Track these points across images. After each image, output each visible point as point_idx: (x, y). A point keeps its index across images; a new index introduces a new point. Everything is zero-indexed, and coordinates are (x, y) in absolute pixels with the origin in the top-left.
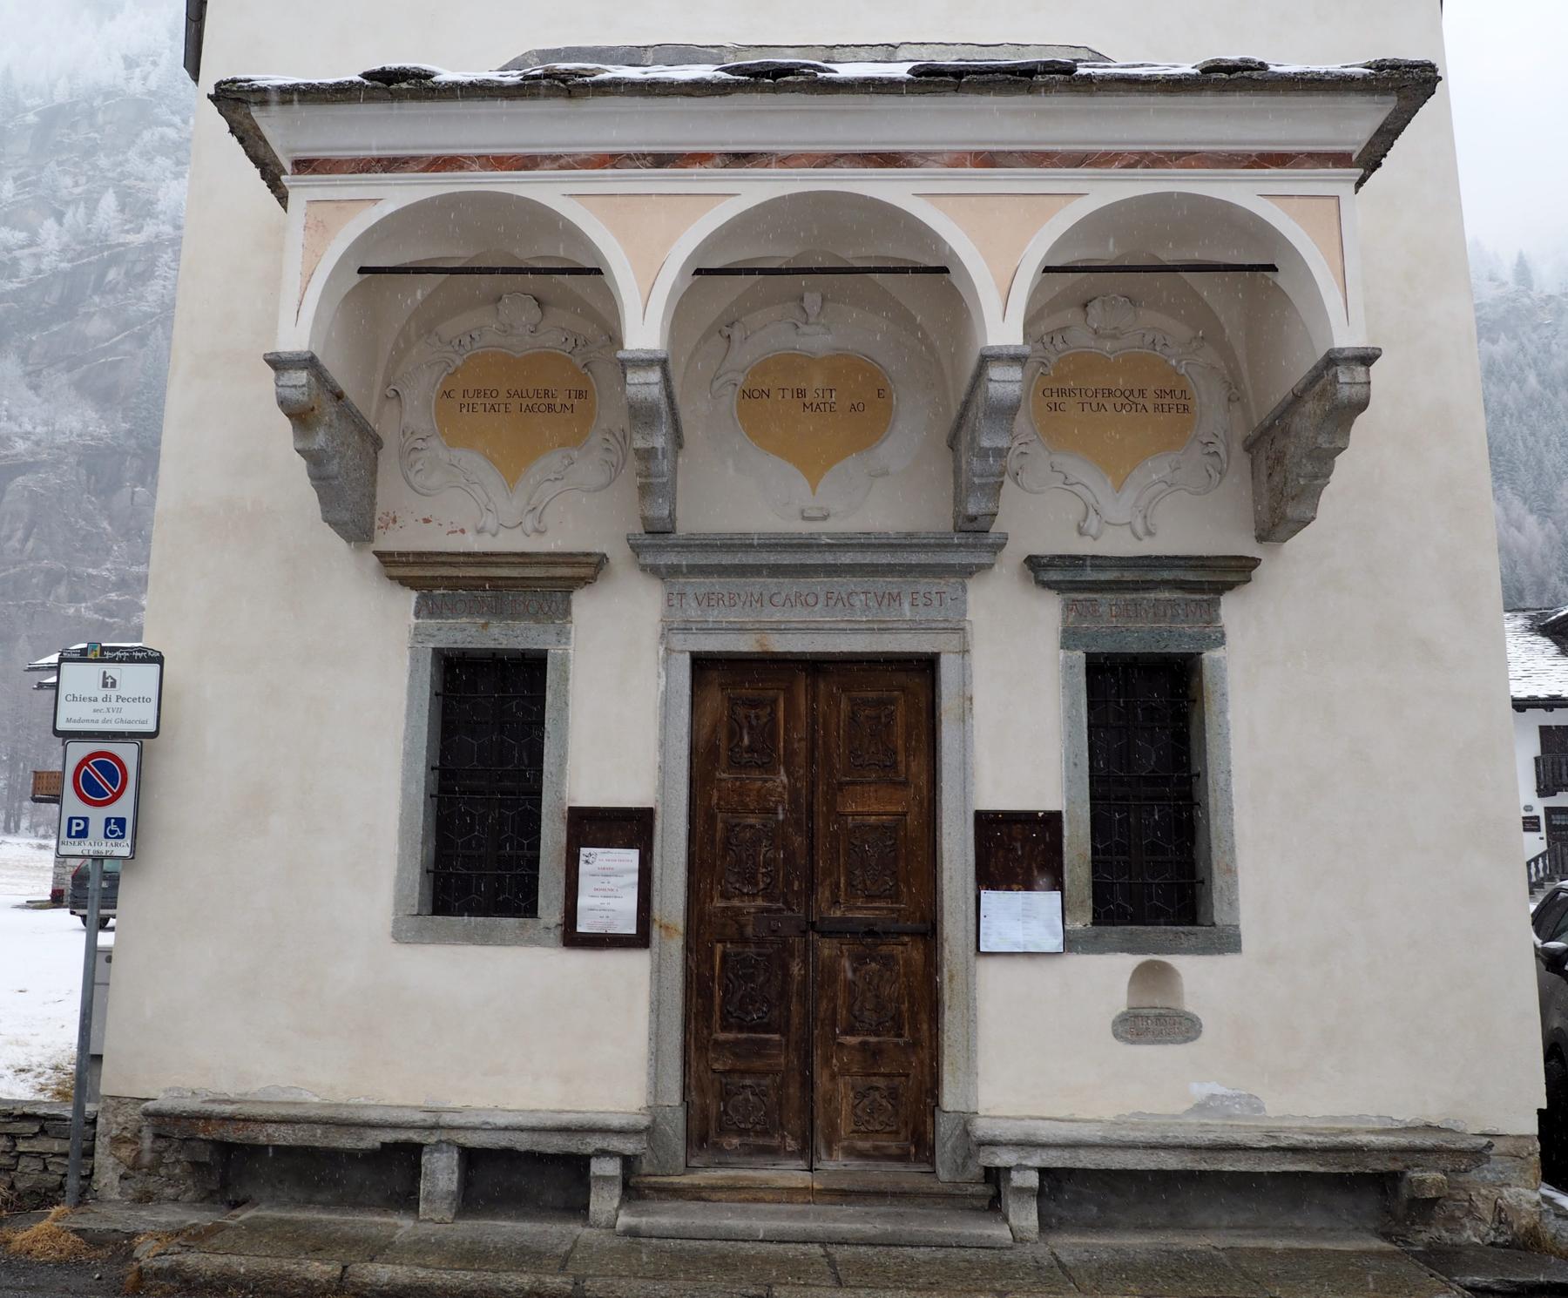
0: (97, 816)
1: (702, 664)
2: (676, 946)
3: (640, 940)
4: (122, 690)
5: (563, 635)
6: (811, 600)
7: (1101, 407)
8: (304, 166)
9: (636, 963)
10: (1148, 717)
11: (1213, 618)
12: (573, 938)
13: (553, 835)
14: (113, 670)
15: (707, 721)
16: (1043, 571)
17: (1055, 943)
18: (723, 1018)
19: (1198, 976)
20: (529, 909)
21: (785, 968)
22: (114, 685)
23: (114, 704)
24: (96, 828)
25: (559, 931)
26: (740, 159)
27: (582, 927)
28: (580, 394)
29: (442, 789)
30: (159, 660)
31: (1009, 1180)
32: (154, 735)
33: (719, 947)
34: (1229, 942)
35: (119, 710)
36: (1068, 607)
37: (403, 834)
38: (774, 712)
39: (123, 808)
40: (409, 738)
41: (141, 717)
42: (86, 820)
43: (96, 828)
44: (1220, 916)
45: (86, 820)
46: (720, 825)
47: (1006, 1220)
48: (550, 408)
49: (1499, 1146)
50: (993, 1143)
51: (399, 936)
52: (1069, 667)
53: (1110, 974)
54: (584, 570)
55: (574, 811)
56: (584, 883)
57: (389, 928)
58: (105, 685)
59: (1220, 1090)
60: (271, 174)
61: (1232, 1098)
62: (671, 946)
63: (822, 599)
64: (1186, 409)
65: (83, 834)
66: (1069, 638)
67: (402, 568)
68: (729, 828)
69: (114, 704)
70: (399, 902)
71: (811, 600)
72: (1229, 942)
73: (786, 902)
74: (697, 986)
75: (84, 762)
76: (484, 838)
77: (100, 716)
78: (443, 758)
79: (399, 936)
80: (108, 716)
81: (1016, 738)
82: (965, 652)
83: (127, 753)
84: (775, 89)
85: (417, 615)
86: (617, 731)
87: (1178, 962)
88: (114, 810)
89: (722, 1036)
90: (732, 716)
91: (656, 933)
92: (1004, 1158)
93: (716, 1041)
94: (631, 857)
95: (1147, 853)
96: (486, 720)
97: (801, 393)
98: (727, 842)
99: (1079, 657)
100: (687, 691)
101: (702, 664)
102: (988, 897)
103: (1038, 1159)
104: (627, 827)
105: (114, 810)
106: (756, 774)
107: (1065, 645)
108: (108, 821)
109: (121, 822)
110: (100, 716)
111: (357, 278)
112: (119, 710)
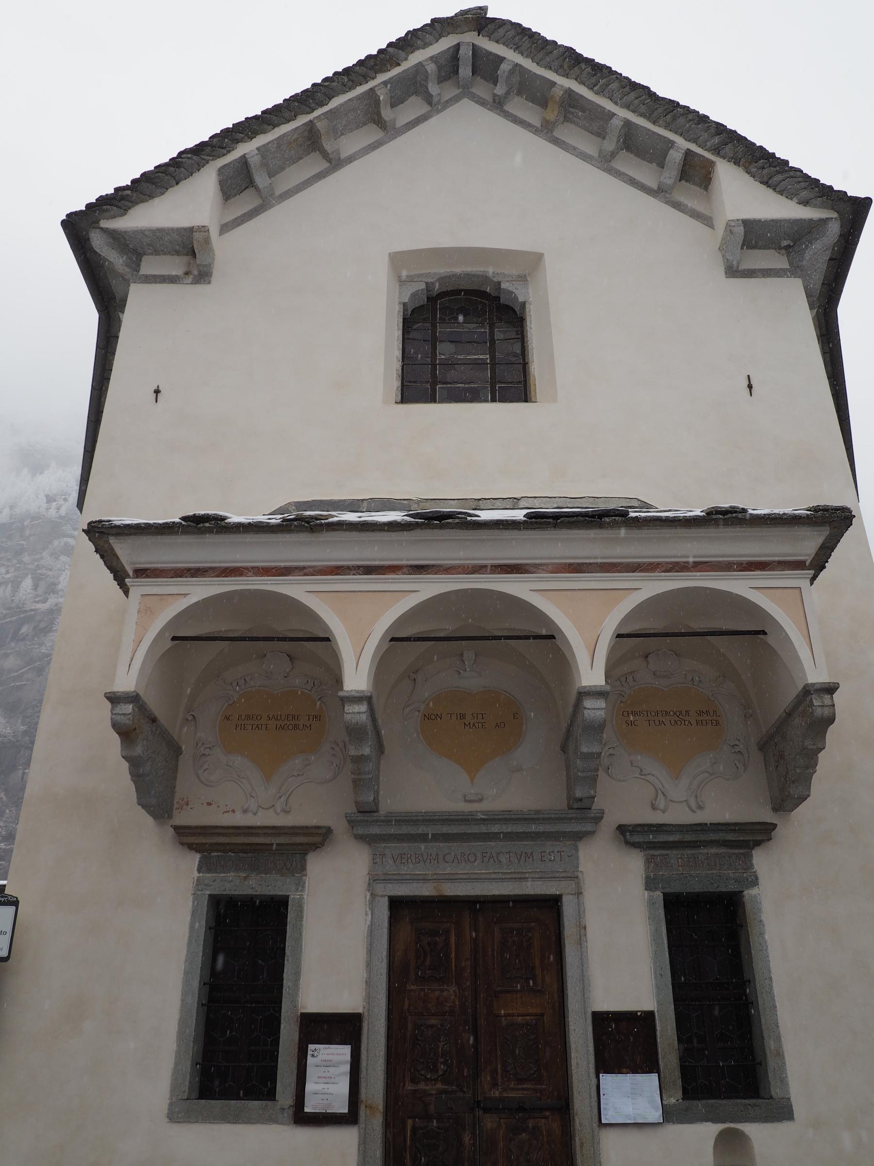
1: (396, 904)
3: (349, 1118)
5: (300, 885)
6: (472, 859)
8: (141, 573)
9: (346, 1139)
10: (709, 938)
11: (748, 865)
12: (303, 1118)
13: (289, 1033)
16: (631, 835)
17: (656, 1115)
20: (270, 1095)
25: (291, 1112)
26: (419, 569)
34: (782, 1112)
36: (648, 861)
48: (296, 727)
51: (173, 1117)
52: (651, 903)
54: (316, 839)
62: (376, 1123)
64: (718, 723)
66: (650, 884)
70: (174, 1088)
71: (472, 859)
72: (782, 1112)
79: (173, 1117)
81: (618, 959)
82: (579, 894)
84: (441, 527)
86: (335, 957)
87: (751, 1129)
91: (362, 1112)
96: (245, 942)
97: (462, 716)
99: (658, 895)
101: (396, 904)
102: (607, 1080)
104: (341, 1028)
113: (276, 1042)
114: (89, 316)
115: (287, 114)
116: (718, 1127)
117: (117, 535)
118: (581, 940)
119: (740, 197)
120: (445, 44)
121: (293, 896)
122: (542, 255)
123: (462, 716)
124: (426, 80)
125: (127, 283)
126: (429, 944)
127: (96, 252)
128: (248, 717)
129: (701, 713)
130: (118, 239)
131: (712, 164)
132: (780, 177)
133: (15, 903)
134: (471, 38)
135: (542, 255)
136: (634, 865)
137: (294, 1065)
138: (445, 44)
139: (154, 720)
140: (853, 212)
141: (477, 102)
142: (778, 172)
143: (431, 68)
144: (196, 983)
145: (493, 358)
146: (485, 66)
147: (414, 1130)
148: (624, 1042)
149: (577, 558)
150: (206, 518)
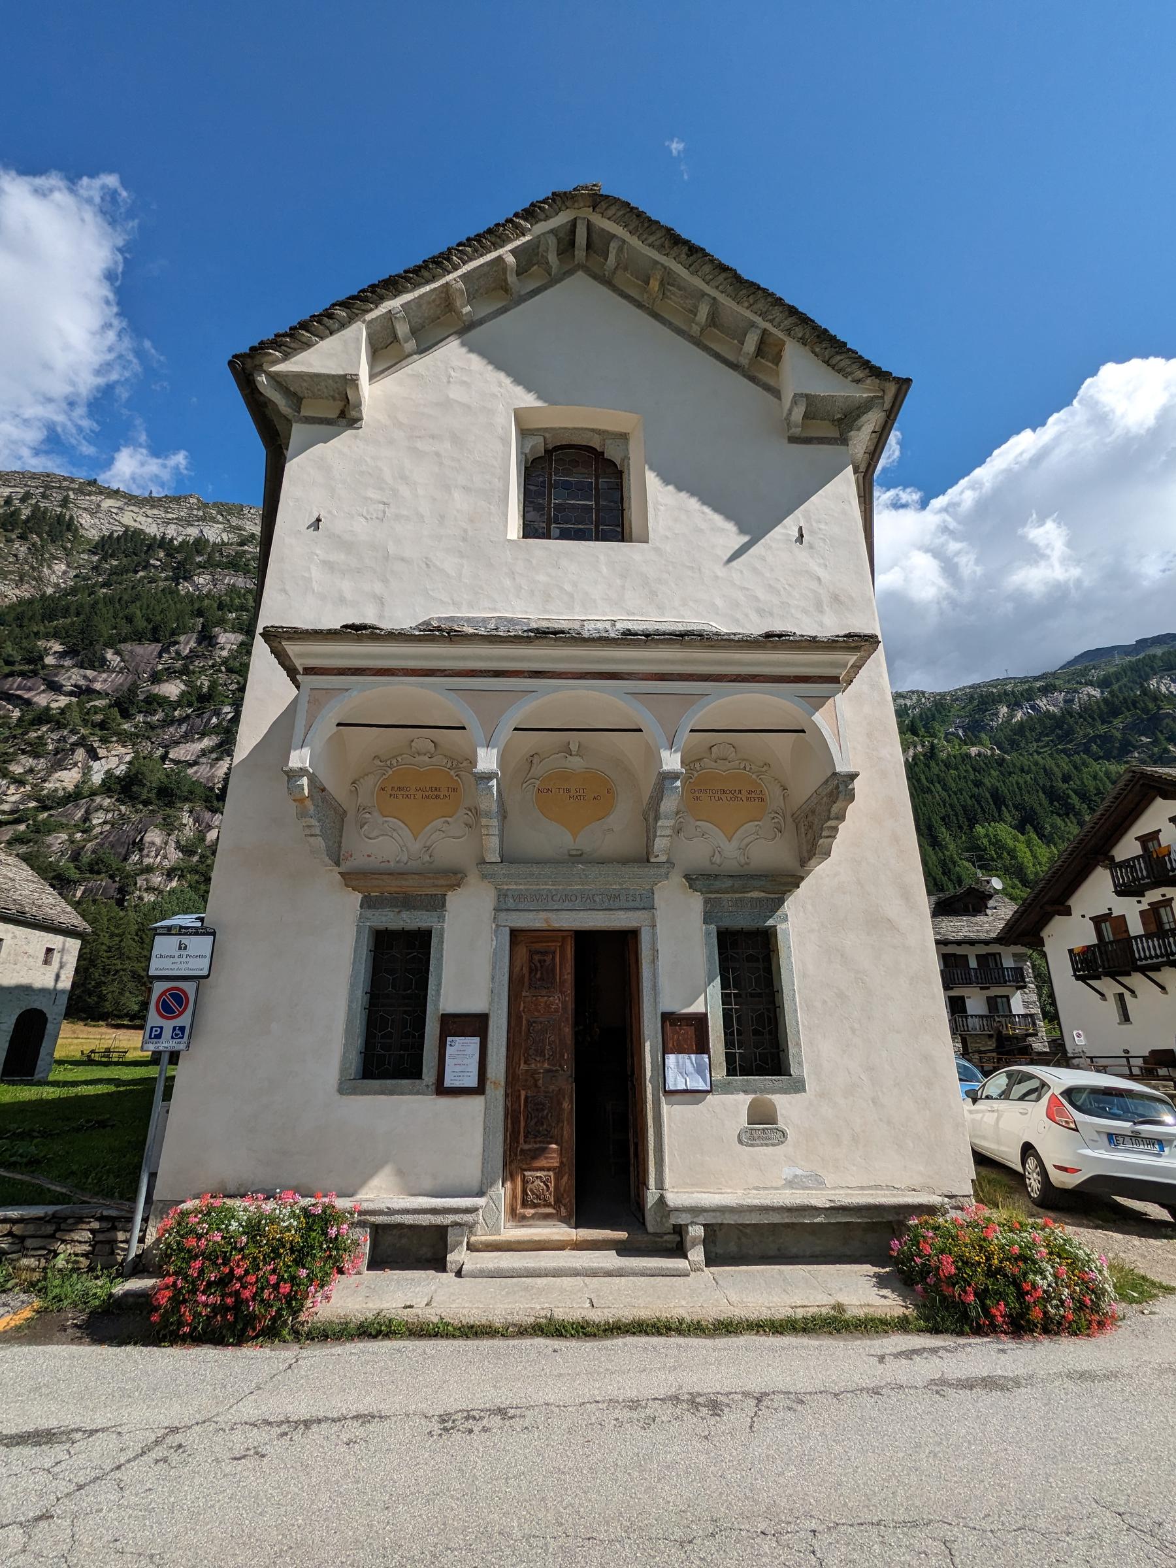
0: (168, 1025)
2: (500, 1093)
3: (480, 1090)
4: (190, 951)
5: (441, 918)
6: (573, 898)
7: (720, 799)
8: (309, 671)
9: (476, 1104)
10: (749, 962)
12: (441, 1090)
13: (432, 1029)
14: (185, 940)
15: (518, 964)
16: (693, 880)
18: (526, 1137)
19: (783, 1104)
20: (418, 1075)
21: (560, 1103)
22: (185, 948)
23: (184, 959)
24: (167, 1033)
25: (434, 1087)
27: (448, 1083)
28: (454, 790)
29: (371, 1004)
30: (214, 934)
31: (687, 1232)
32: (207, 977)
33: (523, 1093)
34: (799, 1087)
35: (187, 963)
37: (348, 1031)
38: (554, 958)
39: (184, 1020)
40: (354, 976)
41: (200, 966)
42: (161, 1028)
43: (167, 1033)
44: (794, 1070)
45: (161, 1028)
46: (524, 1022)
47: (686, 1258)
48: (438, 797)
49: (411, 345)
50: (677, 1210)
51: (341, 1091)
52: (708, 934)
53: (735, 1105)
54: (454, 877)
56: (448, 1061)
57: (336, 1086)
58: (180, 948)
59: (799, 1172)
60: (292, 672)
61: (806, 1177)
62: (496, 1092)
63: (579, 898)
64: (763, 800)
65: (159, 1036)
67: (351, 879)
68: (530, 1024)
69: (184, 959)
70: (343, 1070)
71: (573, 898)
72: (799, 1087)
73: (560, 1066)
74: (512, 1116)
75: (164, 993)
76: (394, 1039)
77: (175, 967)
78: (366, 1049)
79: (341, 1091)
80: (181, 966)
81: (681, 975)
82: (654, 926)
83: (189, 987)
84: (556, 640)
85: (361, 907)
86: (469, 971)
88: (178, 1022)
89: (526, 1147)
90: (531, 960)
91: (489, 1087)
92: (683, 1219)
93: (522, 1150)
94: (477, 1039)
95: (759, 1045)
96: (398, 967)
97: (568, 790)
98: (528, 1032)
99: (713, 928)
100: (508, 948)
101: (515, 934)
102: (671, 1059)
103: (701, 1219)
105: (178, 1022)
106: (544, 992)
107: (705, 922)
108: (174, 1029)
109: (182, 1029)
110: (175, 967)
111: (335, 729)
112: (187, 963)
113: (422, 1036)
114: (258, 451)
115: (426, 274)
116: (749, 1098)
117: (288, 639)
118: (654, 960)
119: (801, 373)
120: (561, 219)
121: (436, 926)
122: (1070, 914)
123: (568, 790)
124: (547, 251)
125: (289, 423)
126: (540, 961)
127: (261, 394)
128: (399, 789)
129: (750, 792)
130: (278, 380)
131: (784, 343)
132: (839, 358)
133: (214, 934)
134: (587, 213)
135: (1070, 914)
136: (696, 903)
137: (436, 1054)
138: (561, 219)
139: (323, 790)
140: (904, 384)
141: (590, 275)
142: (837, 353)
143: (552, 242)
144: (359, 993)
145: (597, 504)
146: (597, 243)
147: (526, 1098)
149: (643, 1273)
150: (364, 627)
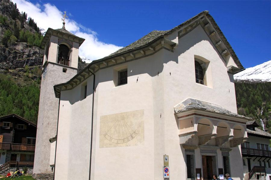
55: (196, 169)
82: (217, 156)
101: (202, 156)
148: (221, 172)
